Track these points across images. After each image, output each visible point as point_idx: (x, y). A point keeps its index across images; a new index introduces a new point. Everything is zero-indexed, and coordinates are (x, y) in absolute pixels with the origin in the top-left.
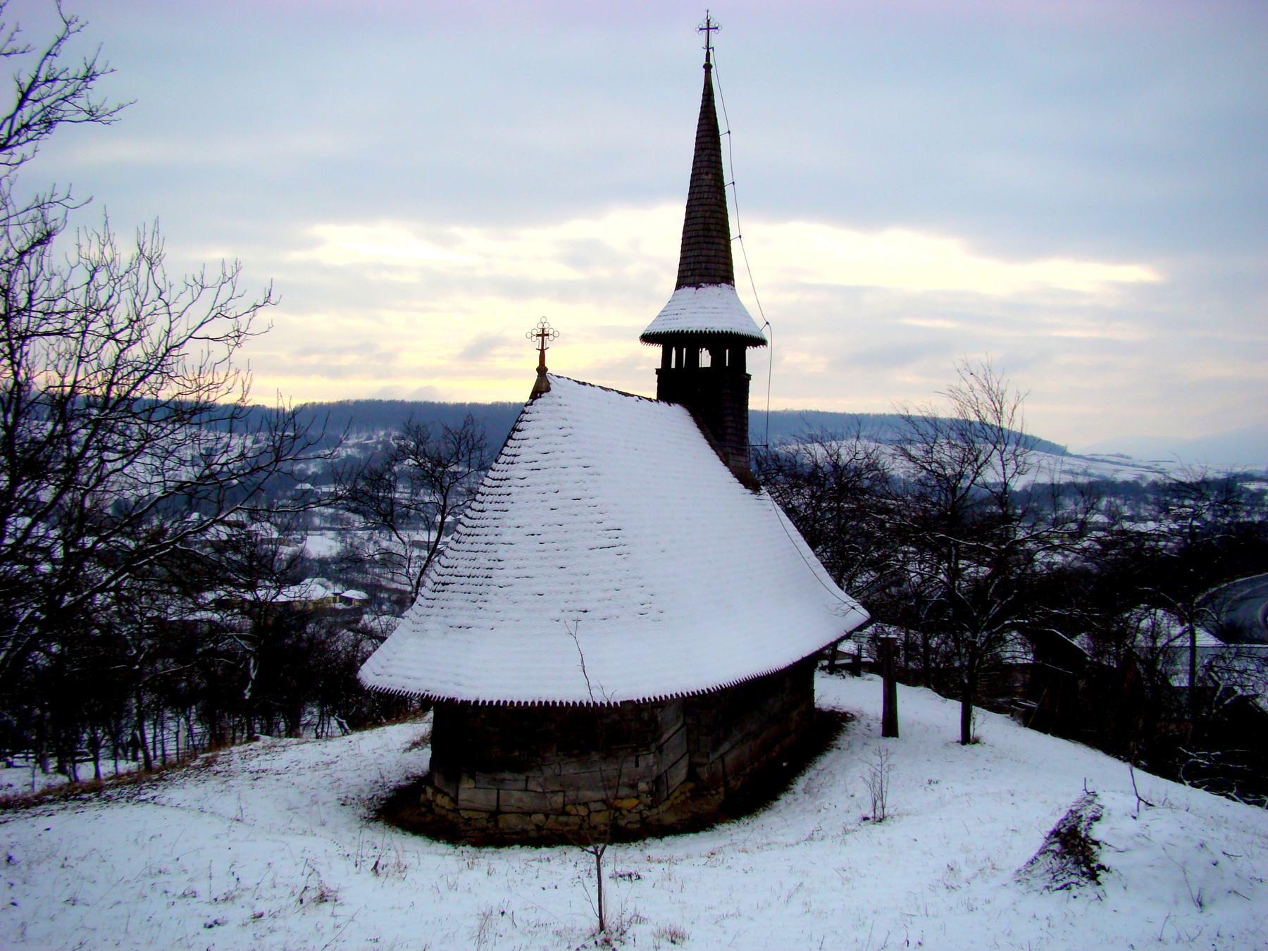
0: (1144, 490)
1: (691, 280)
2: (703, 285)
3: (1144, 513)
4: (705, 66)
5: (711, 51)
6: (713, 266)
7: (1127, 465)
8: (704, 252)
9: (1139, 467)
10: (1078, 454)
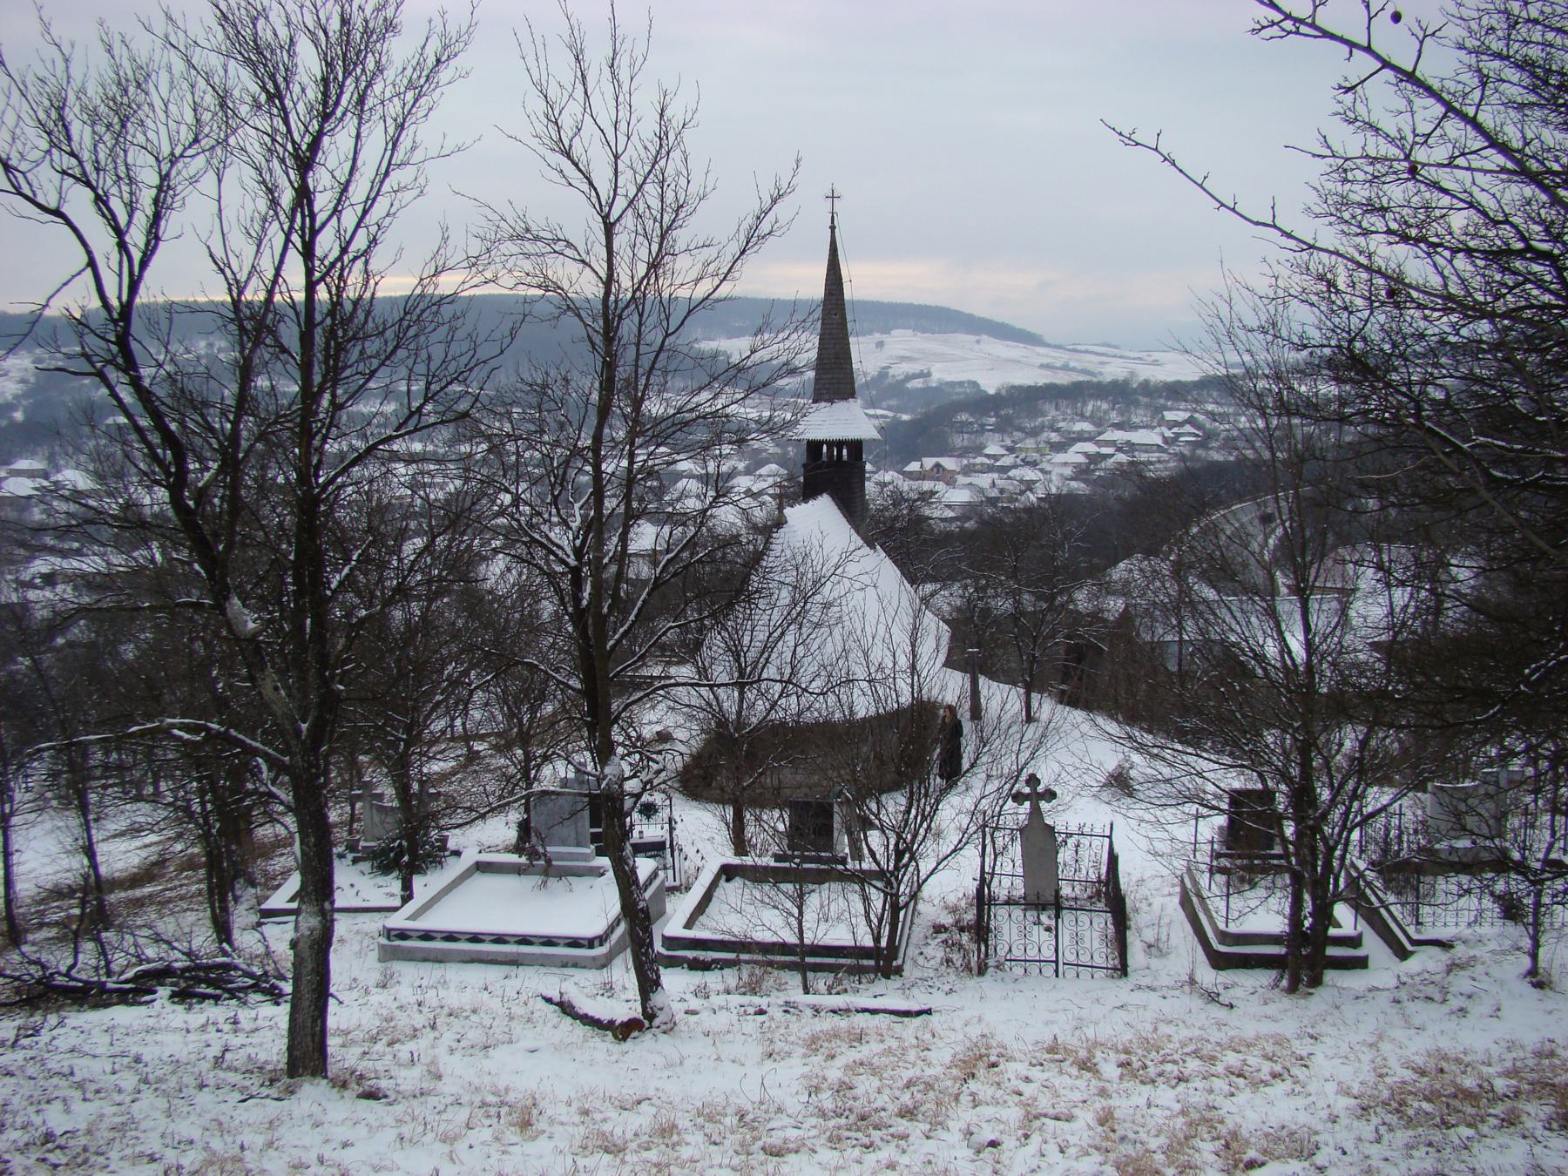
0: (1135, 391)
3: (1135, 419)
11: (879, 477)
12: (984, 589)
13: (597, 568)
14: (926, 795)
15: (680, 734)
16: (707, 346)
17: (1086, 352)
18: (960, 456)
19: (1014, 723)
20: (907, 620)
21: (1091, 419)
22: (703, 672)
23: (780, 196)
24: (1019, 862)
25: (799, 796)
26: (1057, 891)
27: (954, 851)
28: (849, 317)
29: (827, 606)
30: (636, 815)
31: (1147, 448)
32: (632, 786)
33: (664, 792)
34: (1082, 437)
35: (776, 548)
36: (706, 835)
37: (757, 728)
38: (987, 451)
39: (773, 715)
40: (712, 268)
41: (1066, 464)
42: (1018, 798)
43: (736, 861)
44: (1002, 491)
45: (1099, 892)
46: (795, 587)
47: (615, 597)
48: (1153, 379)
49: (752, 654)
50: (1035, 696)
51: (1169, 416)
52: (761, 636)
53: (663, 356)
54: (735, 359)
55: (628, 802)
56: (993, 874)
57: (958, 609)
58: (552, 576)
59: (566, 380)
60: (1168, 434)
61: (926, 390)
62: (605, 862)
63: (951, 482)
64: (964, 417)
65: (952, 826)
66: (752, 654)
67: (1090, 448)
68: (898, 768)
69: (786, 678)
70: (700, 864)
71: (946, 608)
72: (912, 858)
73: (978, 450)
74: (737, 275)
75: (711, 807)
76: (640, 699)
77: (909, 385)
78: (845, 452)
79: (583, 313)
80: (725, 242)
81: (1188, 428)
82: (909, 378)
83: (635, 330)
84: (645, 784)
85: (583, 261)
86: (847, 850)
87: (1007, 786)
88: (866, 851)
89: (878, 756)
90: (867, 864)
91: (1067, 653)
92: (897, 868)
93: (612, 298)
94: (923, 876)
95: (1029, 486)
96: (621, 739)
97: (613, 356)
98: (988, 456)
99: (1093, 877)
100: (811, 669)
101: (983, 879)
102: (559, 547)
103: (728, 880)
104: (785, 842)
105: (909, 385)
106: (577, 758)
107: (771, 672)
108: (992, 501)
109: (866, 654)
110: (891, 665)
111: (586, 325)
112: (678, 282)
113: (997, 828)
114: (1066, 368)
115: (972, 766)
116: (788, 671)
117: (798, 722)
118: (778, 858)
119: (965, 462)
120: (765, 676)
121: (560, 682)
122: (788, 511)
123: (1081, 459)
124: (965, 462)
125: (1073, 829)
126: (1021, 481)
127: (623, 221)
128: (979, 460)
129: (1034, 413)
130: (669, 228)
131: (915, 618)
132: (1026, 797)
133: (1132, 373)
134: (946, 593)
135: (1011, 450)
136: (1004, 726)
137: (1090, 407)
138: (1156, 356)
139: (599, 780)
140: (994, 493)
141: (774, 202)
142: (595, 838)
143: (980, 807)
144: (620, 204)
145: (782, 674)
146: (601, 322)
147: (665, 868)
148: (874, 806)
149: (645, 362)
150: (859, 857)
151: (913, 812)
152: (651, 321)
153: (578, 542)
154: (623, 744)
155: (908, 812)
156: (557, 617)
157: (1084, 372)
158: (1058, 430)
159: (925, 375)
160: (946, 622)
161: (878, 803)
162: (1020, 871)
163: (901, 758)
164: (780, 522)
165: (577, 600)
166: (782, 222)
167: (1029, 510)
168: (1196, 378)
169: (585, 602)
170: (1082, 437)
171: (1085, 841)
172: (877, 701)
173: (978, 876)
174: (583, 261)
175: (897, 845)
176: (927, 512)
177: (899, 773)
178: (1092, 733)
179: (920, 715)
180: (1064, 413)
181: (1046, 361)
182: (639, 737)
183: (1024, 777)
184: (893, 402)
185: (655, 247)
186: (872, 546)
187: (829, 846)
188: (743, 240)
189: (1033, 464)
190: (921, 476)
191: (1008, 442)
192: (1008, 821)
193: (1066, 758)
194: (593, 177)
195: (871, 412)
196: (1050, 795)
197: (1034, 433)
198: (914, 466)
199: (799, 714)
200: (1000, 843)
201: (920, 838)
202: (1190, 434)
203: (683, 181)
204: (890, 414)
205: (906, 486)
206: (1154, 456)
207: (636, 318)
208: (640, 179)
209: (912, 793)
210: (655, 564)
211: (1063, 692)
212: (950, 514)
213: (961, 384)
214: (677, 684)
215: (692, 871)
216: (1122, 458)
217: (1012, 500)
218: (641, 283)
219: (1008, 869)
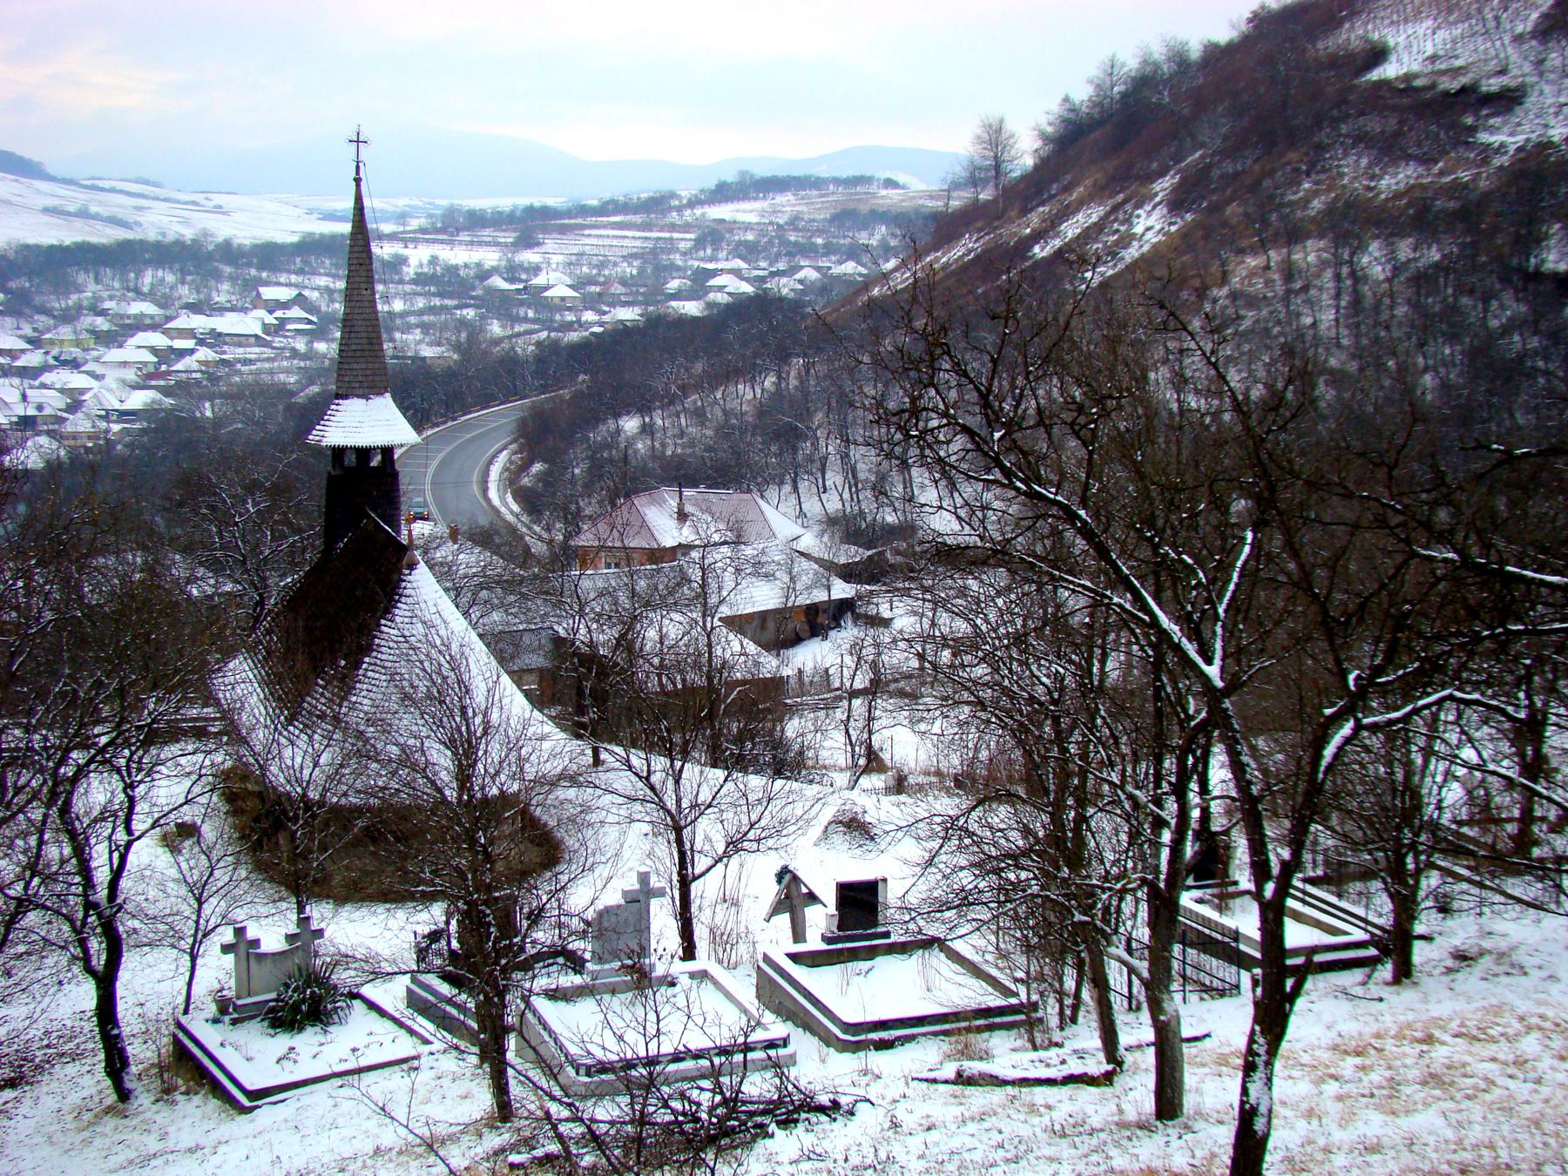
0: (210, 257)
1: (360, 392)
3: (220, 298)
7: (156, 199)
9: (178, 202)
10: (68, 177)
17: (112, 190)
21: (151, 296)
31: (240, 340)
34: (140, 325)
41: (125, 364)
48: (236, 241)
51: (268, 293)
60: (270, 319)
67: (158, 340)
81: (296, 312)
114: (83, 214)
133: (205, 234)
135: (35, 342)
138: (218, 199)
158: (103, 313)
168: (295, 239)
170: (140, 325)
180: (109, 288)
189: (74, 365)
191: (27, 330)
197: (68, 317)
202: (299, 320)
206: (253, 352)
216: (204, 353)
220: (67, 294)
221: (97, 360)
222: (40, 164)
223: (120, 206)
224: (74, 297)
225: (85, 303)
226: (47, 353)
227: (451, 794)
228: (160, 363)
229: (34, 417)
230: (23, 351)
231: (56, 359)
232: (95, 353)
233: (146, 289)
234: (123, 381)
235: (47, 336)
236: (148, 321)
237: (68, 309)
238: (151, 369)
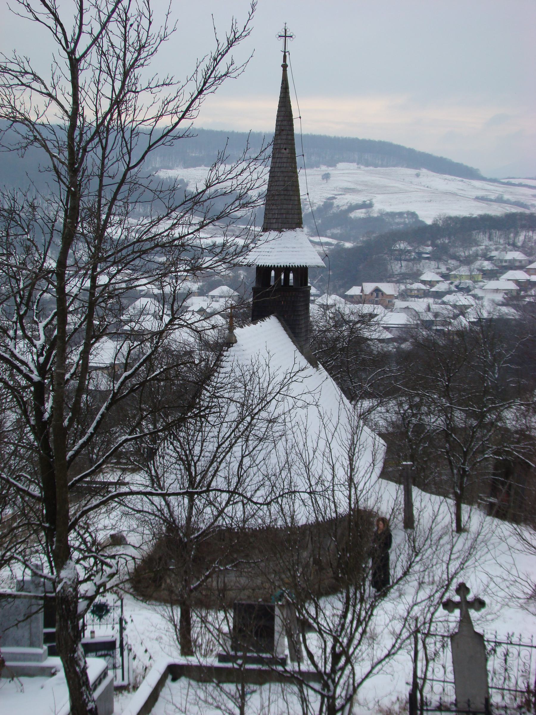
1: (275, 226)
2: (284, 230)
4: (282, 66)
5: (287, 54)
6: (291, 216)
8: (285, 206)
11: (320, 300)
12: (418, 406)
13: (59, 384)
14: (362, 600)
15: (133, 539)
16: (164, 174)
17: (520, 185)
18: (398, 282)
19: (445, 533)
20: (345, 436)
21: (523, 249)
22: (155, 480)
23: (236, 39)
24: (450, 668)
25: (244, 598)
26: (487, 700)
27: (388, 656)
28: (298, 151)
29: (272, 421)
30: (88, 616)
32: (86, 588)
33: (116, 593)
34: (513, 266)
35: (226, 366)
36: (154, 635)
37: (205, 533)
38: (424, 277)
39: (220, 521)
40: (171, 107)
41: (497, 291)
42: (449, 605)
43: (181, 660)
44: (436, 315)
45: (528, 702)
46: (243, 405)
47: (76, 409)
49: (202, 464)
50: (465, 508)
52: (211, 447)
53: (125, 188)
54: (192, 189)
55: (82, 605)
56: (425, 679)
57: (393, 424)
58: (15, 391)
59: (33, 207)
61: (368, 220)
62: (56, 661)
63: (389, 305)
64: (402, 245)
65: (386, 631)
66: (202, 464)
67: (521, 275)
68: (335, 573)
69: (232, 488)
70: (147, 663)
71: (382, 423)
72: (348, 661)
73: (415, 276)
74: (194, 113)
75: (159, 608)
76: (97, 506)
77: (352, 215)
78: (291, 276)
79: (49, 145)
80: (183, 82)
82: (353, 208)
83: (99, 162)
84: (99, 587)
85: (49, 95)
86: (287, 652)
87: (438, 595)
88: (305, 653)
89: (317, 562)
90: (306, 666)
91: (496, 468)
92: (334, 670)
93: (77, 132)
94: (358, 679)
95: (462, 310)
96: (77, 544)
97: (78, 186)
98: (424, 282)
99: (522, 686)
100: (256, 479)
101: (415, 684)
102: (23, 363)
103: (174, 679)
104: (229, 643)
105: (352, 215)
106: (34, 561)
107: (219, 482)
108: (427, 325)
109: (307, 467)
110: (330, 478)
111: (52, 156)
112: (140, 118)
113: (428, 635)
114: (500, 200)
115: (405, 574)
116: (234, 480)
117: (243, 528)
118: (222, 658)
119: (402, 287)
120: (213, 484)
121: (19, 490)
122: (237, 331)
123: (512, 286)
124: (402, 287)
125: (502, 638)
126: (455, 306)
127: (88, 58)
128: (416, 285)
129: (470, 242)
130: (132, 66)
131: (353, 434)
132: (457, 605)
134: (383, 409)
135: (445, 277)
136: (435, 537)
137: (521, 238)
139: (55, 583)
140: (430, 317)
141: (231, 44)
142: (48, 638)
143: (413, 613)
144: (85, 41)
145: (229, 483)
146: (66, 154)
147: (114, 667)
148: (312, 611)
149: (108, 194)
150: (297, 657)
151: (349, 616)
152: (113, 155)
153: (42, 359)
154: (78, 549)
155: (344, 616)
156: (19, 425)
157: (518, 204)
159: (365, 206)
160: (380, 435)
161: (317, 607)
162: (451, 677)
163: (339, 565)
164: (230, 342)
165: (40, 413)
166: (237, 64)
167: (461, 333)
169: (47, 415)
170: (513, 266)
171: (513, 650)
172: (317, 510)
173: (411, 680)
174: (49, 95)
175: (333, 648)
176: (366, 334)
177: (337, 578)
178: (519, 546)
179: (357, 525)
180: (497, 243)
181: (480, 193)
182: (94, 542)
183: (454, 586)
184: (337, 231)
185: (118, 85)
186: (314, 364)
187: (270, 647)
188: (200, 80)
189: (467, 290)
190: (361, 300)
191: (443, 270)
192: (439, 628)
193: (495, 571)
194: (59, 12)
195: (316, 239)
196: (479, 604)
197: (468, 261)
198: (355, 291)
199: (244, 521)
200: (431, 649)
201: (355, 642)
203: (145, 23)
204: (334, 242)
205: (347, 308)
207: (99, 150)
208: (104, 18)
209: (348, 598)
210: (114, 377)
211: (492, 505)
212: (388, 335)
213: (401, 214)
214: (132, 493)
215: (140, 670)
217: (446, 323)
218: (104, 118)
219: (439, 674)
220: (469, 247)
221: (481, 288)
222: (477, 170)
223: (523, 195)
224: (474, 249)
225: (480, 252)
226: (451, 283)
227: (290, 525)
228: (520, 290)
229: (433, 321)
230: (438, 282)
231: (457, 287)
232: (481, 284)
233: (519, 244)
234: (493, 301)
235: (453, 273)
236: (517, 264)
237: (469, 256)
238: (514, 294)
